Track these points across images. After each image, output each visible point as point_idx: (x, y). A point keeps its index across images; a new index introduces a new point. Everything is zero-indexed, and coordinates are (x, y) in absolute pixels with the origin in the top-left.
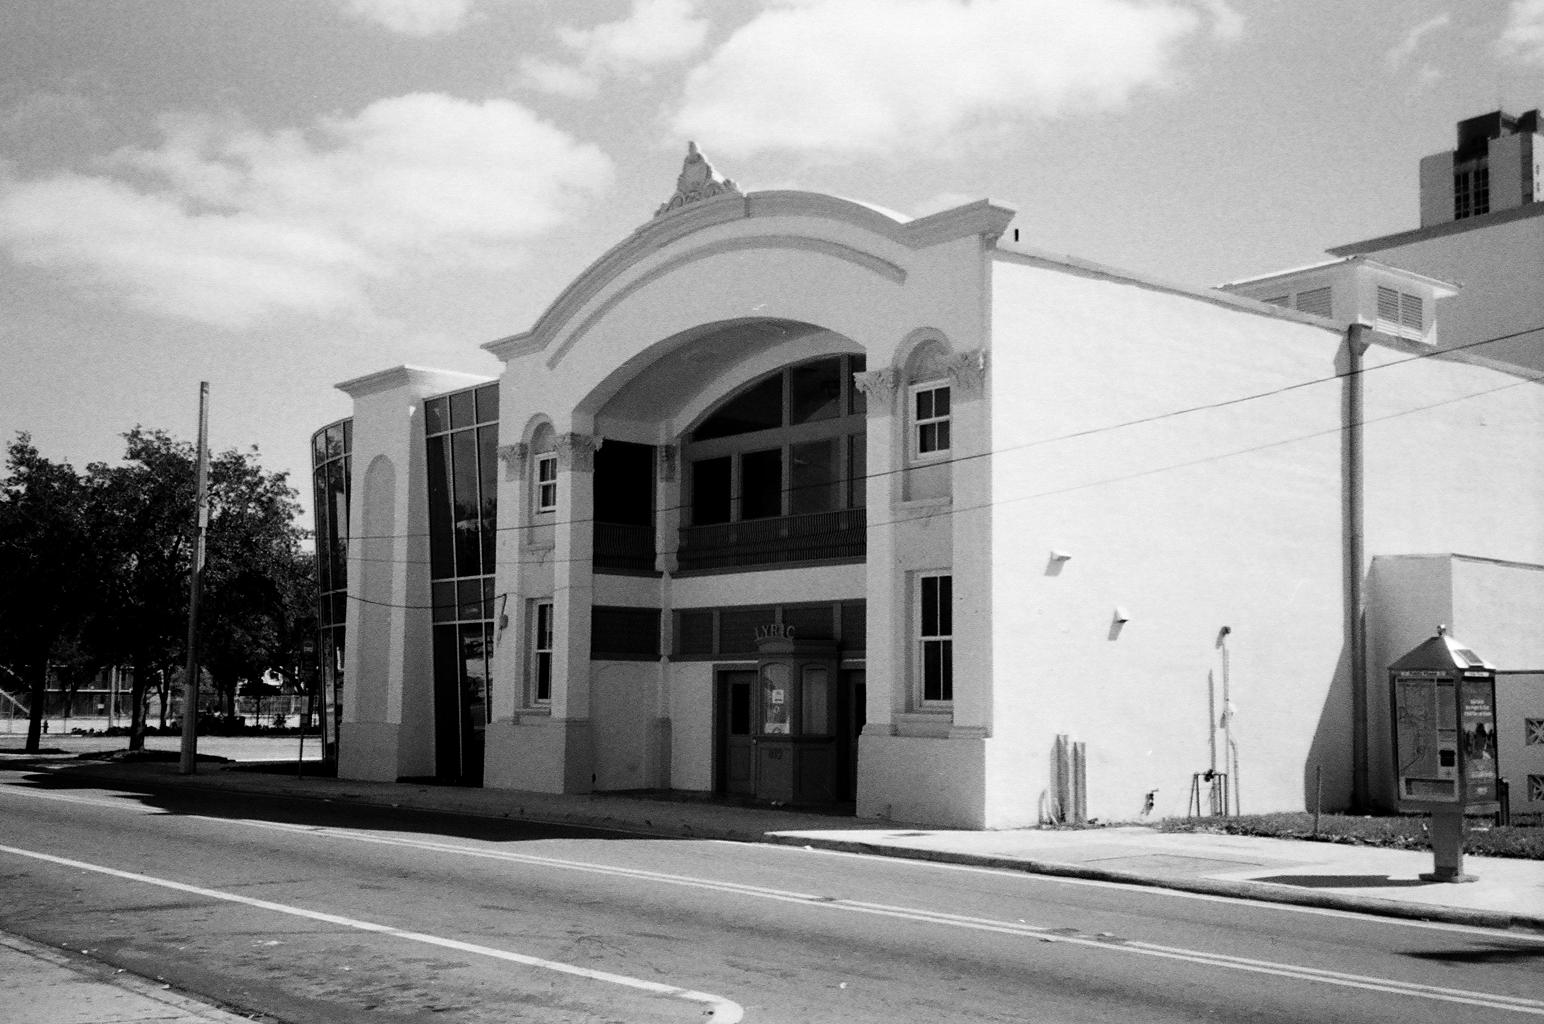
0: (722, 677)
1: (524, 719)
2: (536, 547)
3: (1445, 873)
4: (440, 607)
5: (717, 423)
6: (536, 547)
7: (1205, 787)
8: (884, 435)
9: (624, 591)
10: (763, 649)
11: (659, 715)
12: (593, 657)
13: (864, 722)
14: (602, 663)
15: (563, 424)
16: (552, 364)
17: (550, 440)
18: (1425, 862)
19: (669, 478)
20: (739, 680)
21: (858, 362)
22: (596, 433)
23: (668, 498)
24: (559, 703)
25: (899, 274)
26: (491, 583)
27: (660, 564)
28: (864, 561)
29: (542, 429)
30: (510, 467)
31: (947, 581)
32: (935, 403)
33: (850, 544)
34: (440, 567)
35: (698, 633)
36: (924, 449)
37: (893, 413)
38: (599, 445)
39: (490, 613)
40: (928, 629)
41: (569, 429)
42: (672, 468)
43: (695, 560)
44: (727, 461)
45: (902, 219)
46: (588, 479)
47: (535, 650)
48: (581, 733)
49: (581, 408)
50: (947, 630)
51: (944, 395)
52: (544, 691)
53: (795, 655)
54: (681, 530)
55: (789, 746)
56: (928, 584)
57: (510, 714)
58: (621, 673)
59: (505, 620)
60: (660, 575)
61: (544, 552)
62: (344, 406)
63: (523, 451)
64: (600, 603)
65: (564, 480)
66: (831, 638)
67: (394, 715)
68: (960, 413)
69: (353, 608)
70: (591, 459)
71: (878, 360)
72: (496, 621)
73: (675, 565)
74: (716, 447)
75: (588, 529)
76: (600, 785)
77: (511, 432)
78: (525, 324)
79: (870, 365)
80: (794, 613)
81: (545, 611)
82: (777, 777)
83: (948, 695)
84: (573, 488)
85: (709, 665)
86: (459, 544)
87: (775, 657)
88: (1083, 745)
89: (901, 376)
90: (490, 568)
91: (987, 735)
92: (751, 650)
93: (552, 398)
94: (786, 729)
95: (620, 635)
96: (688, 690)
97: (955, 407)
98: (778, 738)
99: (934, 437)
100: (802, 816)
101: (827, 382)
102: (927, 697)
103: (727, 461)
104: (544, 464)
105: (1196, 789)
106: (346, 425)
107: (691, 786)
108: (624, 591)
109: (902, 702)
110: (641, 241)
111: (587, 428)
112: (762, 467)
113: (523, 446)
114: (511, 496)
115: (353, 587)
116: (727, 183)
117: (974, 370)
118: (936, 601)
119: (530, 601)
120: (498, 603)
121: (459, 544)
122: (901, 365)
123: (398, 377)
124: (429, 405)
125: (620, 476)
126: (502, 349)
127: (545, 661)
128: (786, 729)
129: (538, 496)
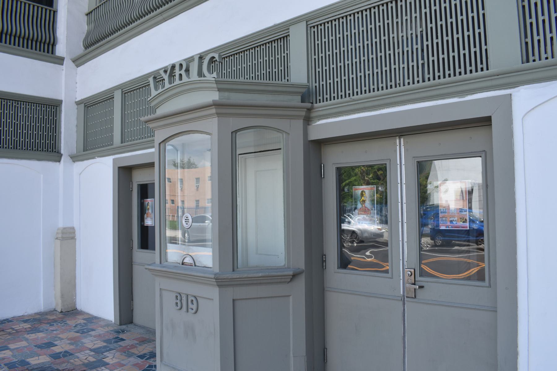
0: (125, 173)
11: (61, 225)
12: (491, 117)
20: (139, 178)
27: (61, 49)
55: (214, 292)
60: (60, 61)
73: (80, 50)
94: (205, 256)
98: (187, 272)
128: (205, 256)
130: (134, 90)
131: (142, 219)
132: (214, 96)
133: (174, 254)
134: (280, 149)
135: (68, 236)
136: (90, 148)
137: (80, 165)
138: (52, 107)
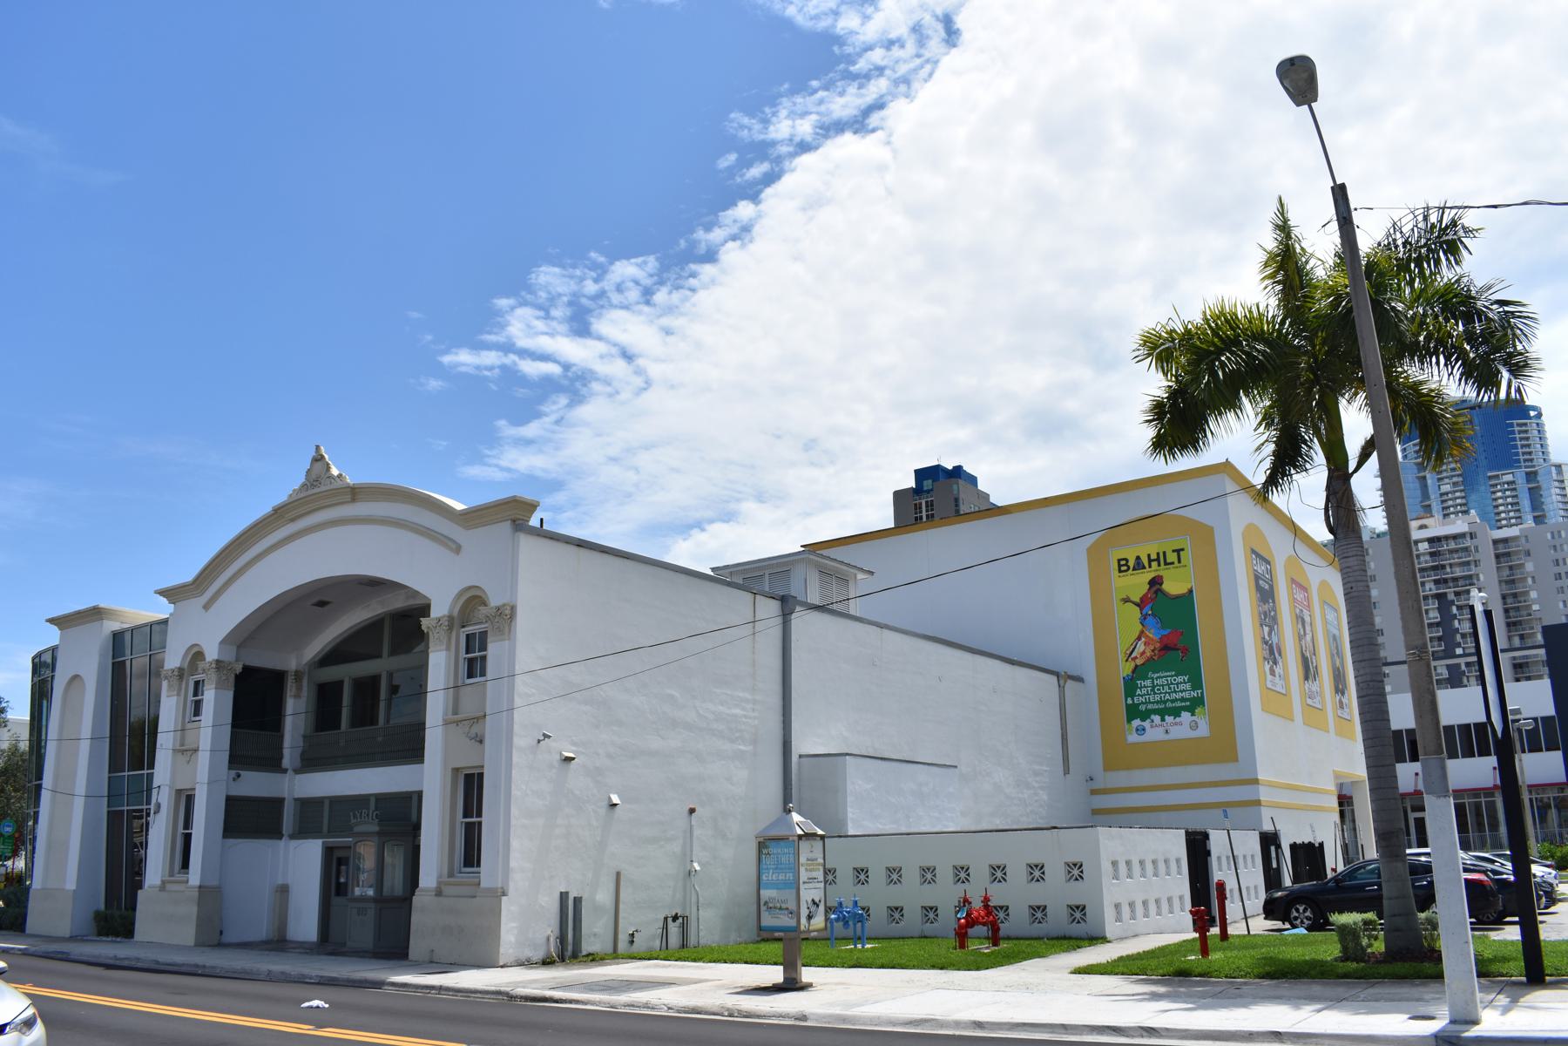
0: (328, 851)
1: (169, 887)
2: (186, 751)
3: (791, 985)
4: (112, 796)
5: (333, 656)
6: (186, 751)
7: (674, 928)
8: (440, 664)
9: (256, 784)
10: (356, 829)
11: (280, 882)
12: (225, 836)
13: (417, 885)
14: (232, 841)
15: (212, 653)
16: (206, 607)
17: (201, 665)
18: (775, 974)
19: (297, 696)
20: (338, 854)
21: (425, 610)
22: (237, 660)
23: (296, 712)
24: (195, 876)
25: (457, 549)
26: (150, 777)
27: (286, 762)
28: (422, 761)
29: (197, 655)
30: (170, 686)
31: (481, 775)
32: (475, 643)
33: (410, 748)
34: (115, 765)
35: (315, 817)
36: (470, 676)
37: (448, 649)
38: (239, 668)
39: (149, 803)
40: (466, 814)
41: (216, 657)
42: (299, 689)
43: (312, 761)
44: (340, 684)
45: (459, 506)
46: (230, 695)
47: (181, 830)
48: (210, 896)
49: (223, 642)
50: (479, 814)
51: (484, 635)
52: (185, 864)
53: (379, 834)
54: (304, 736)
55: (372, 905)
56: (469, 779)
57: (158, 882)
58: (247, 848)
59: (158, 806)
60: (285, 771)
61: (192, 753)
62: (52, 636)
63: (181, 673)
64: (234, 793)
65: (209, 696)
66: (400, 817)
67: (71, 884)
68: (494, 650)
69: (46, 796)
70: (232, 679)
71: (439, 610)
72: (152, 807)
73: (298, 763)
74: (346, 673)
75: (227, 730)
76: (227, 938)
77: (173, 659)
78: (188, 576)
79: (433, 615)
80: (382, 799)
81: (190, 800)
82: (362, 930)
83: (479, 865)
84: (216, 702)
85: (320, 842)
86: (130, 743)
87: (365, 835)
88: (578, 901)
89: (452, 623)
90: (151, 765)
91: (504, 894)
92: (346, 830)
93: (208, 631)
94: (371, 892)
95: (249, 819)
96: (301, 863)
97: (490, 646)
98: (363, 899)
99: (475, 668)
100: (392, 963)
101: (405, 626)
102: (466, 865)
103: (340, 684)
104: (197, 683)
105: (665, 927)
106: (54, 649)
107: (301, 938)
108: (256, 784)
109: (446, 871)
110: (280, 514)
111: (229, 656)
112: (367, 688)
113: (181, 669)
114: (169, 710)
115: (47, 781)
116: (340, 476)
117: (506, 616)
118: (471, 787)
119: (179, 792)
120: (155, 792)
121: (130, 743)
122: (456, 613)
123: (95, 614)
124: (117, 637)
125: (255, 698)
126: (171, 594)
127: (187, 839)
128: (371, 892)
129: (190, 709)
130: (338, 803)
131: (338, 877)
132: (376, 829)
133: (357, 891)
134: (618, 874)
135: (284, 890)
136: (304, 830)
137: (294, 843)
138: (278, 803)
